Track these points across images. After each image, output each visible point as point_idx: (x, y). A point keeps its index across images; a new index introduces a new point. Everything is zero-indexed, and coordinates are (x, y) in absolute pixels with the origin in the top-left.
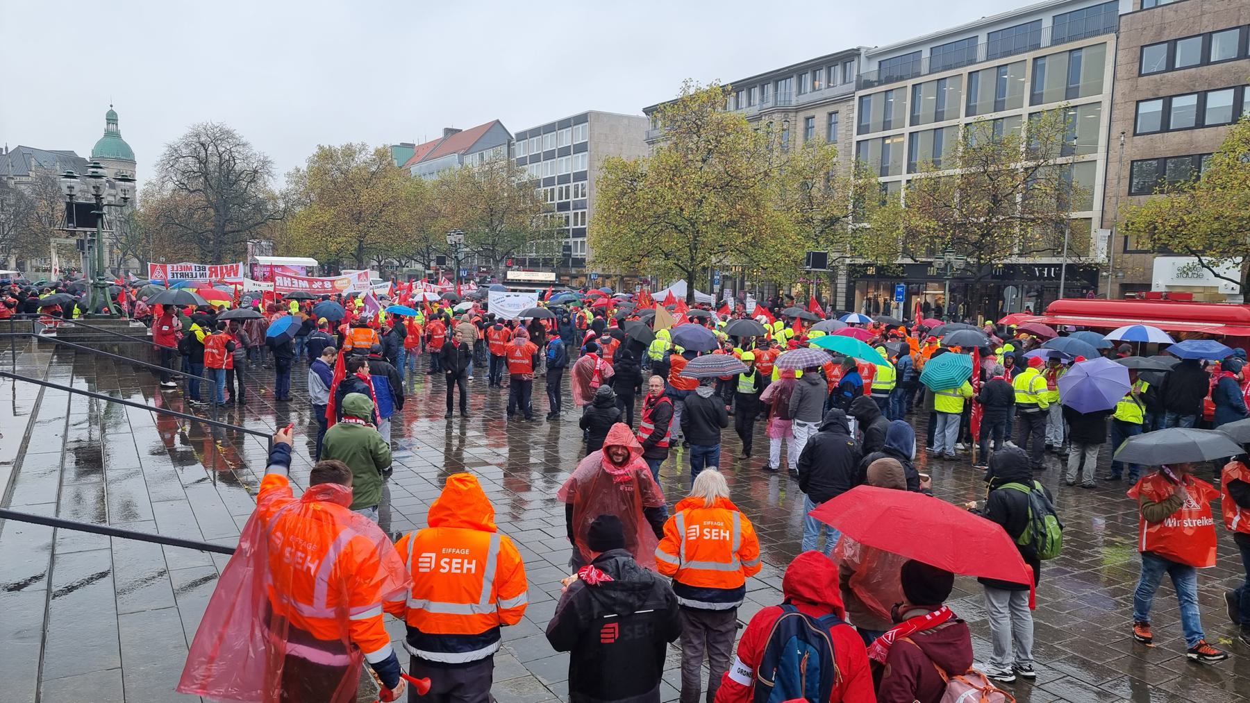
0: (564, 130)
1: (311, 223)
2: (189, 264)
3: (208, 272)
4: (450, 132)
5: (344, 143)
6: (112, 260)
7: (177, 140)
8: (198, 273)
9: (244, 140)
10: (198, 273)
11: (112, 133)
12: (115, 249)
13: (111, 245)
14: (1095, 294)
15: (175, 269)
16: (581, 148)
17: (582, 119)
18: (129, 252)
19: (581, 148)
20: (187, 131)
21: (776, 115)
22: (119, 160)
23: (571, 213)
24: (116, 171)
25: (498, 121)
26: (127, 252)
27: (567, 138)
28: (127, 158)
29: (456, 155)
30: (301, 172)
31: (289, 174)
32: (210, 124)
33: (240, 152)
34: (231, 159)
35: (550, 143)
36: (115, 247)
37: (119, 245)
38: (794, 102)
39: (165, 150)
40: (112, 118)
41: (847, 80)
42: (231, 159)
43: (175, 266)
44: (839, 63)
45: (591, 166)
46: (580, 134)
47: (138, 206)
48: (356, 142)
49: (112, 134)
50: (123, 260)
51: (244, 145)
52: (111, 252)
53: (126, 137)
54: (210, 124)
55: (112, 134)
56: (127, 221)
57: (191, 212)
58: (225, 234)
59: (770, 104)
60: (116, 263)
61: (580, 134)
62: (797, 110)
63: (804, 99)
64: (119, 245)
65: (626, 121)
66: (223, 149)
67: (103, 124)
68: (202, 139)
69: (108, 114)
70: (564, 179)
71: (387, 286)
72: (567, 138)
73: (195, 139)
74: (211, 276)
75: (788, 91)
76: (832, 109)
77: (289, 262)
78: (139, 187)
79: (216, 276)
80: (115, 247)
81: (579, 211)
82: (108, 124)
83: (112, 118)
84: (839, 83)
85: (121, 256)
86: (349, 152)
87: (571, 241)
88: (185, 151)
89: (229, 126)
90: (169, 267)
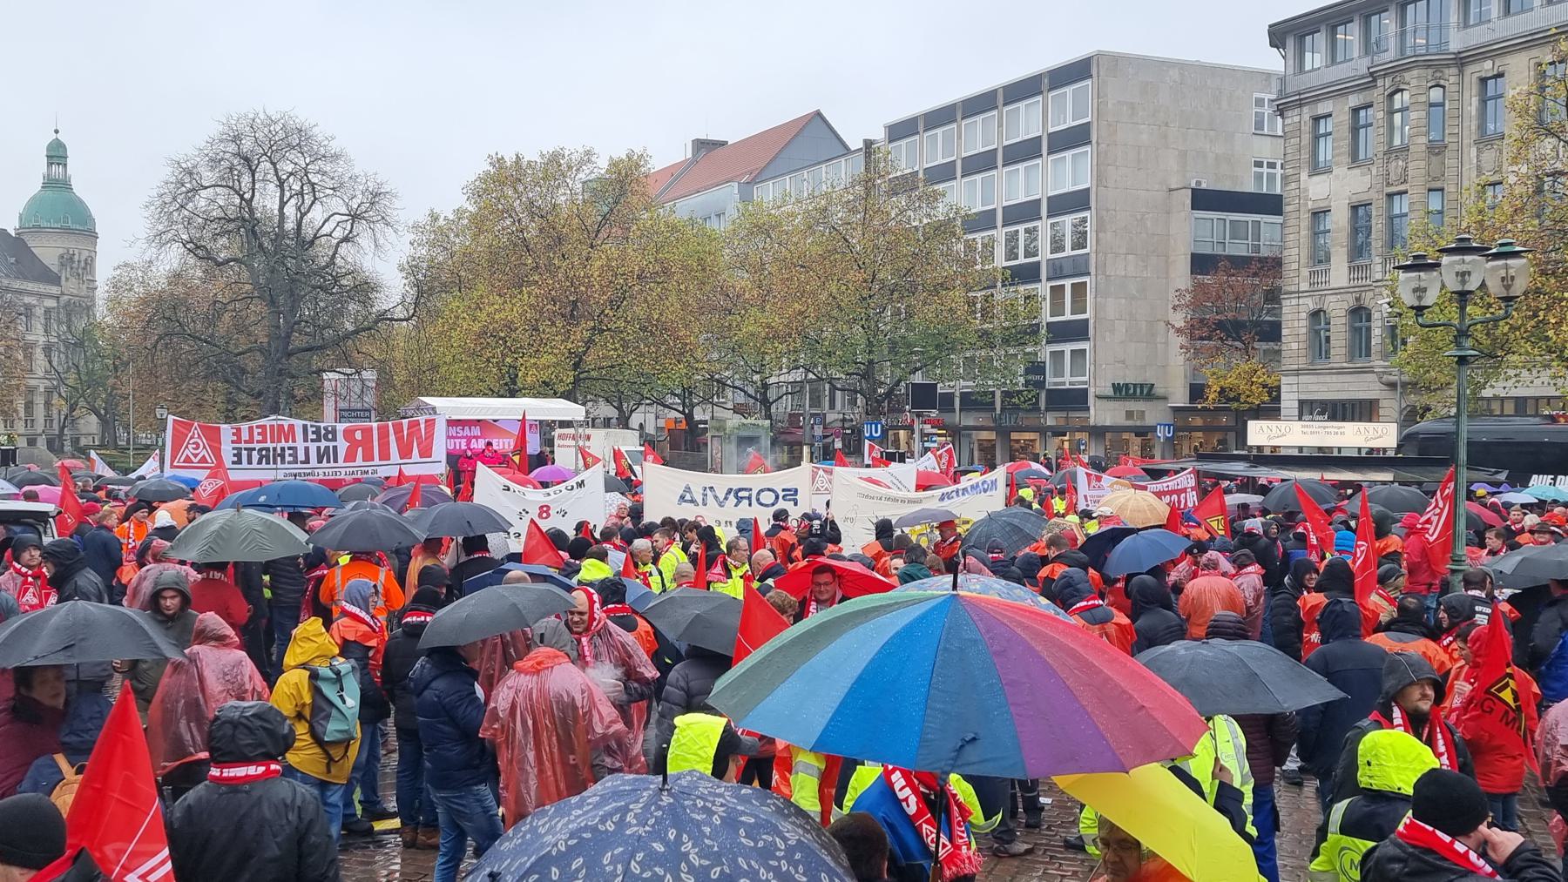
0: (1022, 105)
1: (476, 327)
2: (286, 422)
3: (342, 445)
4: (704, 147)
5: (549, 148)
6: (49, 419)
7: (192, 152)
8: (313, 447)
9: (334, 147)
10: (313, 447)
11: (57, 181)
12: (55, 400)
13: (49, 392)
14: (430, 456)
15: (245, 436)
16: (1075, 138)
17: (1077, 71)
18: (82, 403)
19: (1075, 138)
20: (215, 130)
21: (1415, 72)
22: (67, 231)
23: (1043, 288)
24: (61, 251)
25: (818, 114)
26: (76, 404)
27: (1029, 121)
28: (80, 225)
29: (736, 185)
30: (441, 222)
31: (416, 227)
32: (262, 116)
33: (325, 173)
34: (306, 189)
35: (978, 136)
36: (56, 395)
37: (63, 390)
38: (1457, 42)
39: (167, 173)
40: (57, 154)
41: (1340, 58)
42: (306, 189)
43: (245, 426)
44: (1323, 28)
45: (1100, 177)
46: (1064, 108)
47: (101, 311)
48: (572, 146)
49: (57, 185)
50: (70, 420)
51: (336, 157)
52: (48, 404)
53: (79, 188)
54: (262, 116)
55: (57, 185)
56: (80, 344)
57: (217, 310)
58: (290, 355)
59: (1391, 54)
60: (56, 425)
61: (1064, 108)
62: (1461, 61)
63: (1477, 36)
64: (63, 390)
65: (1174, 74)
66: (290, 168)
67: (39, 168)
68: (247, 145)
69: (50, 147)
70: (1024, 212)
71: (994, 483)
72: (1029, 121)
73: (232, 148)
74: (350, 457)
75: (1434, 20)
76: (1487, 67)
77: (496, 410)
78: (104, 272)
79: (368, 457)
80: (56, 395)
81: (1068, 283)
82: (50, 164)
83: (57, 154)
84: (1356, 55)
85: (65, 410)
86: (555, 167)
87: (1045, 352)
88: (208, 177)
89: (304, 115)
90: (226, 430)
